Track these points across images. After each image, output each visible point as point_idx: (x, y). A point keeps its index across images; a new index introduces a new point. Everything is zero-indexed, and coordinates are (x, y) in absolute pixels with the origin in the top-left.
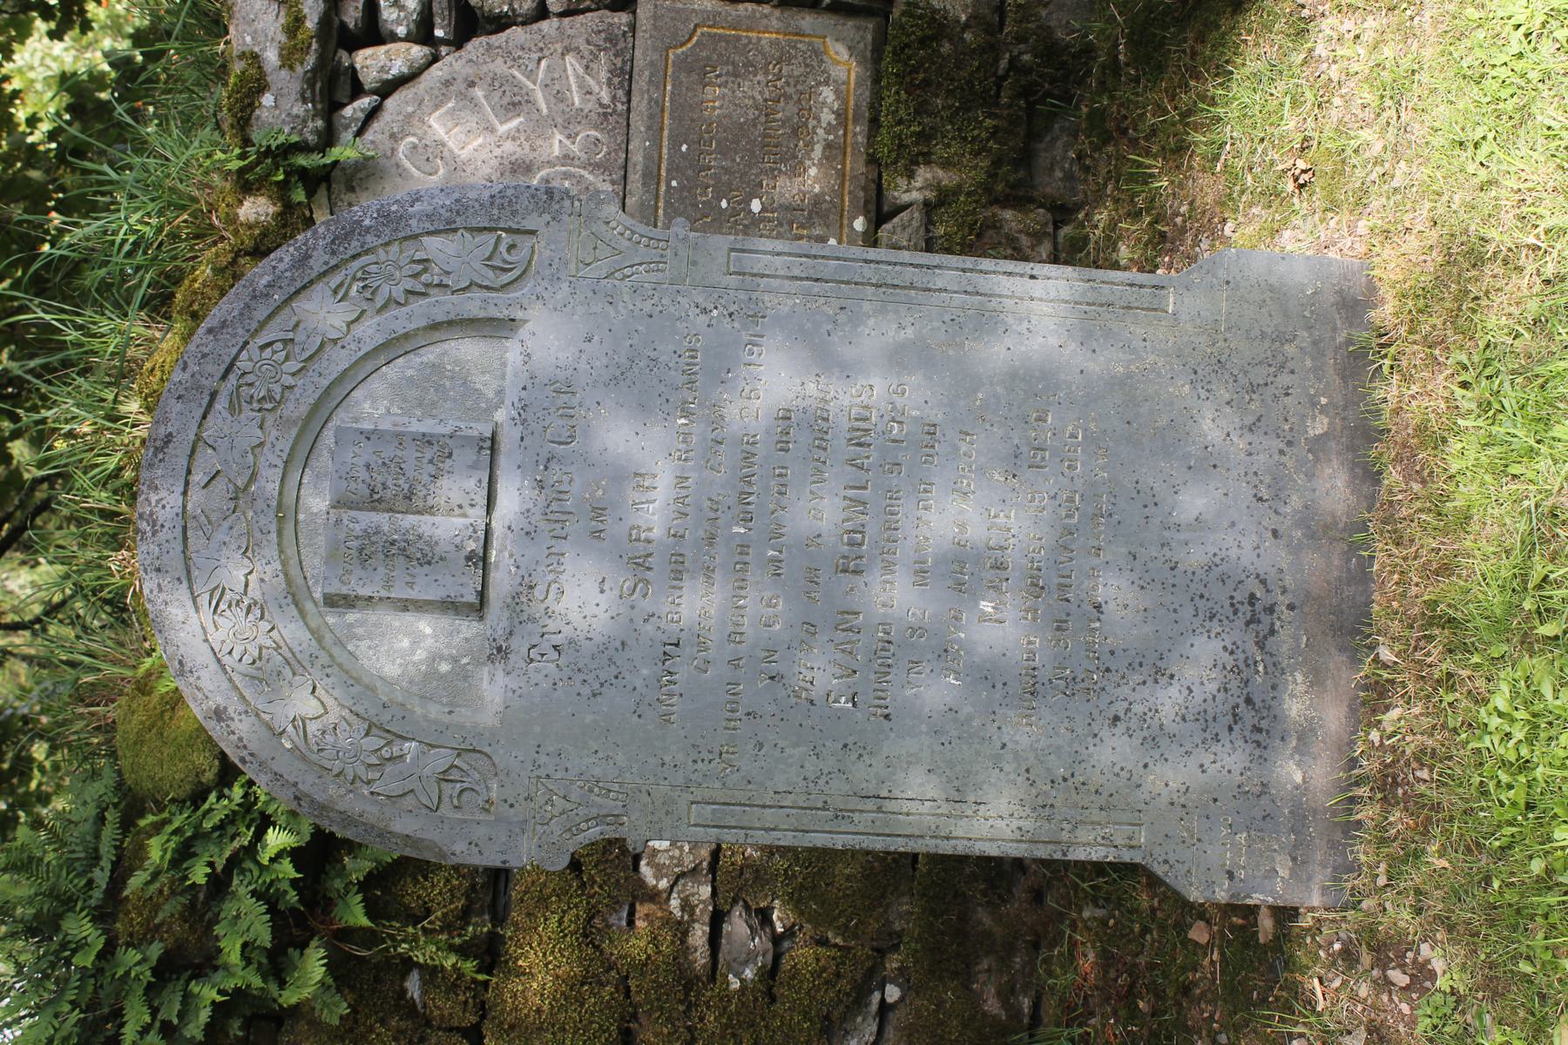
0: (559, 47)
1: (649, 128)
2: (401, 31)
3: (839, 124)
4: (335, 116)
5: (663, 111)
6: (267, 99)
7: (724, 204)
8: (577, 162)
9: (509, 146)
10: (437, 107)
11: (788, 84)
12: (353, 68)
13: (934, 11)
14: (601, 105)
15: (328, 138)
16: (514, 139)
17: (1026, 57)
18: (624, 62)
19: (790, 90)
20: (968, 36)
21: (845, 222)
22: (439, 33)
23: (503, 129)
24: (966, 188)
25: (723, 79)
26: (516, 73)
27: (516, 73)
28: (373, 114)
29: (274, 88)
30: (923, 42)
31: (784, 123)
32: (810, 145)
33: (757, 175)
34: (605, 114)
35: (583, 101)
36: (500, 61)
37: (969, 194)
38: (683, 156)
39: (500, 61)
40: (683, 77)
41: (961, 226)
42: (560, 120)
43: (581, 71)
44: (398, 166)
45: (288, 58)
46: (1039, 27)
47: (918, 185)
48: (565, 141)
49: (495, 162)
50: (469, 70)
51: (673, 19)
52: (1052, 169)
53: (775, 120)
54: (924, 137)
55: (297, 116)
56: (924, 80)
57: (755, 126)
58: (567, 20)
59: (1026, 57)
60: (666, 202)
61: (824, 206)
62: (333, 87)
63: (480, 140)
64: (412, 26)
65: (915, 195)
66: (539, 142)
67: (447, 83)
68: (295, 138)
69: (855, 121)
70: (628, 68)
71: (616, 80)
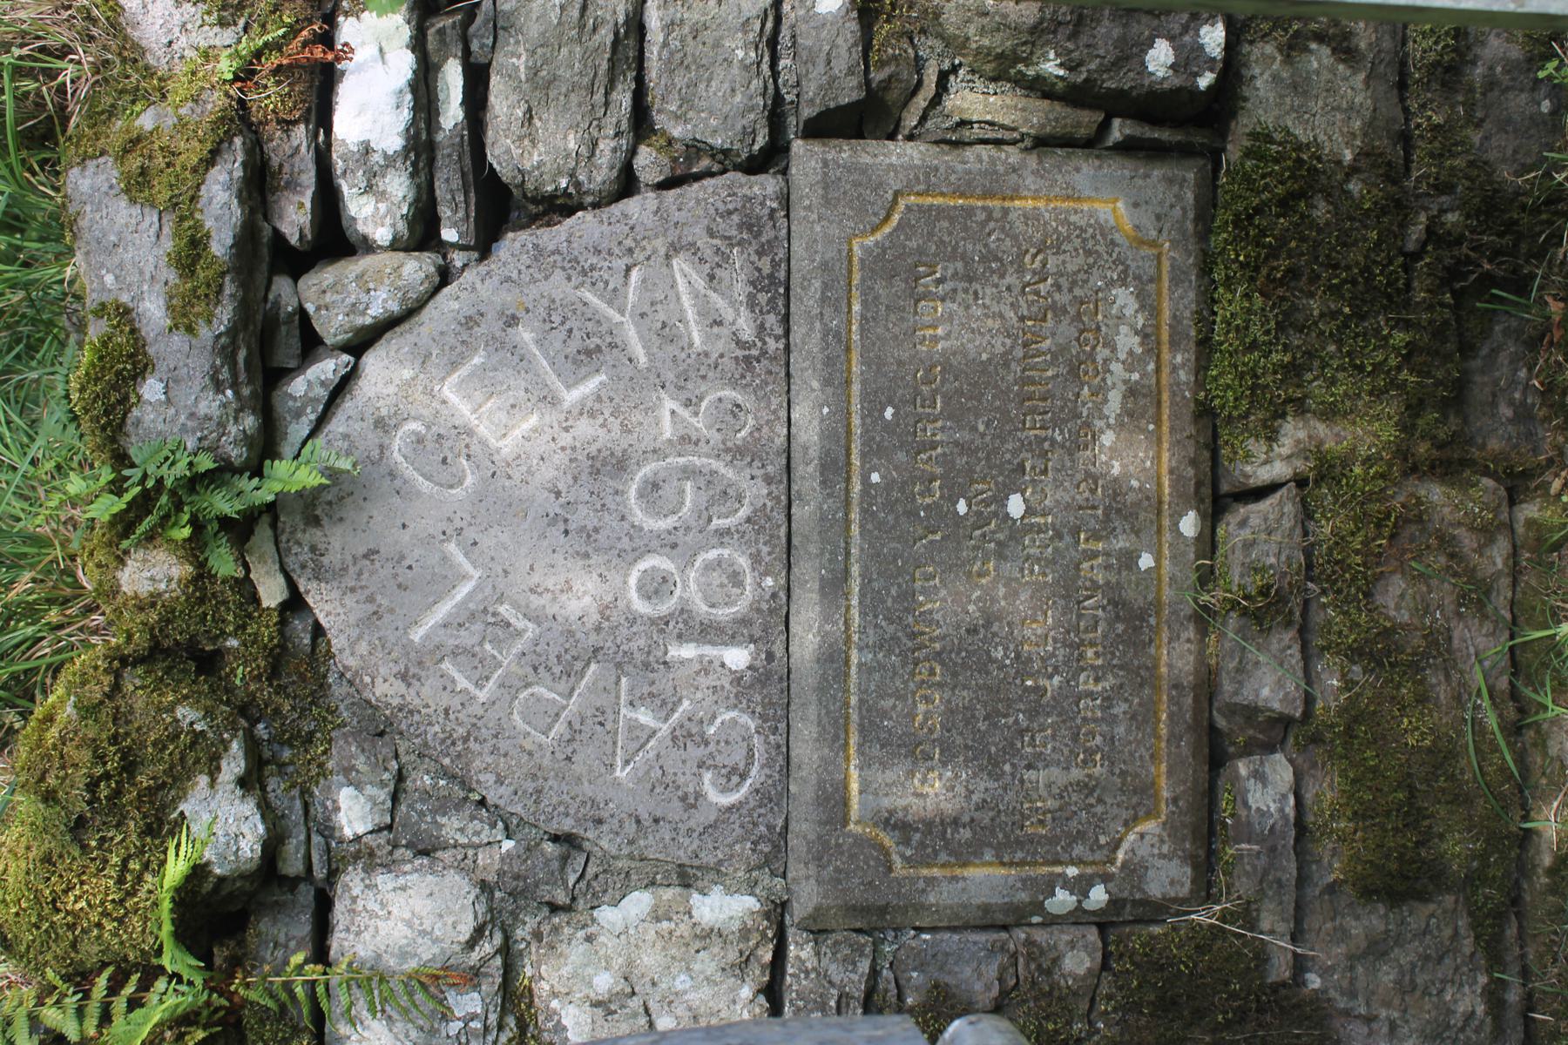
0: (660, 245)
1: (827, 382)
2: (382, 235)
3: (1148, 351)
4: (277, 397)
5: (848, 350)
6: (151, 389)
7: (962, 507)
9: (585, 428)
10: (454, 365)
11: (1058, 287)
12: (302, 312)
13: (1299, 147)
14: (740, 343)
15: (266, 446)
16: (592, 414)
17: (1452, 217)
18: (775, 265)
19: (1063, 298)
20: (1354, 187)
21: (1166, 522)
22: (449, 234)
23: (572, 397)
24: (1363, 451)
25: (949, 286)
26: (589, 296)
27: (589, 296)
28: (342, 387)
29: (162, 367)
30: (1285, 204)
31: (1055, 356)
32: (1100, 391)
33: (1015, 453)
34: (747, 359)
35: (707, 338)
36: (558, 276)
37: (1368, 461)
38: (887, 427)
39: (558, 276)
40: (880, 288)
41: (1361, 520)
42: (670, 376)
43: (700, 284)
44: (392, 475)
45: (183, 318)
46: (1471, 164)
47: (1285, 451)
48: (680, 410)
49: (560, 458)
50: (507, 297)
51: (856, 184)
52: (1494, 404)
53: (1039, 353)
54: (1293, 371)
55: (208, 418)
56: (1289, 271)
57: (1006, 365)
58: (671, 194)
59: (1452, 217)
60: (864, 511)
61: (1130, 498)
62: (266, 350)
63: (534, 420)
64: (402, 227)
65: (1279, 470)
66: (637, 417)
67: (470, 322)
68: (206, 463)
69: (1174, 345)
70: (782, 275)
71: (763, 298)
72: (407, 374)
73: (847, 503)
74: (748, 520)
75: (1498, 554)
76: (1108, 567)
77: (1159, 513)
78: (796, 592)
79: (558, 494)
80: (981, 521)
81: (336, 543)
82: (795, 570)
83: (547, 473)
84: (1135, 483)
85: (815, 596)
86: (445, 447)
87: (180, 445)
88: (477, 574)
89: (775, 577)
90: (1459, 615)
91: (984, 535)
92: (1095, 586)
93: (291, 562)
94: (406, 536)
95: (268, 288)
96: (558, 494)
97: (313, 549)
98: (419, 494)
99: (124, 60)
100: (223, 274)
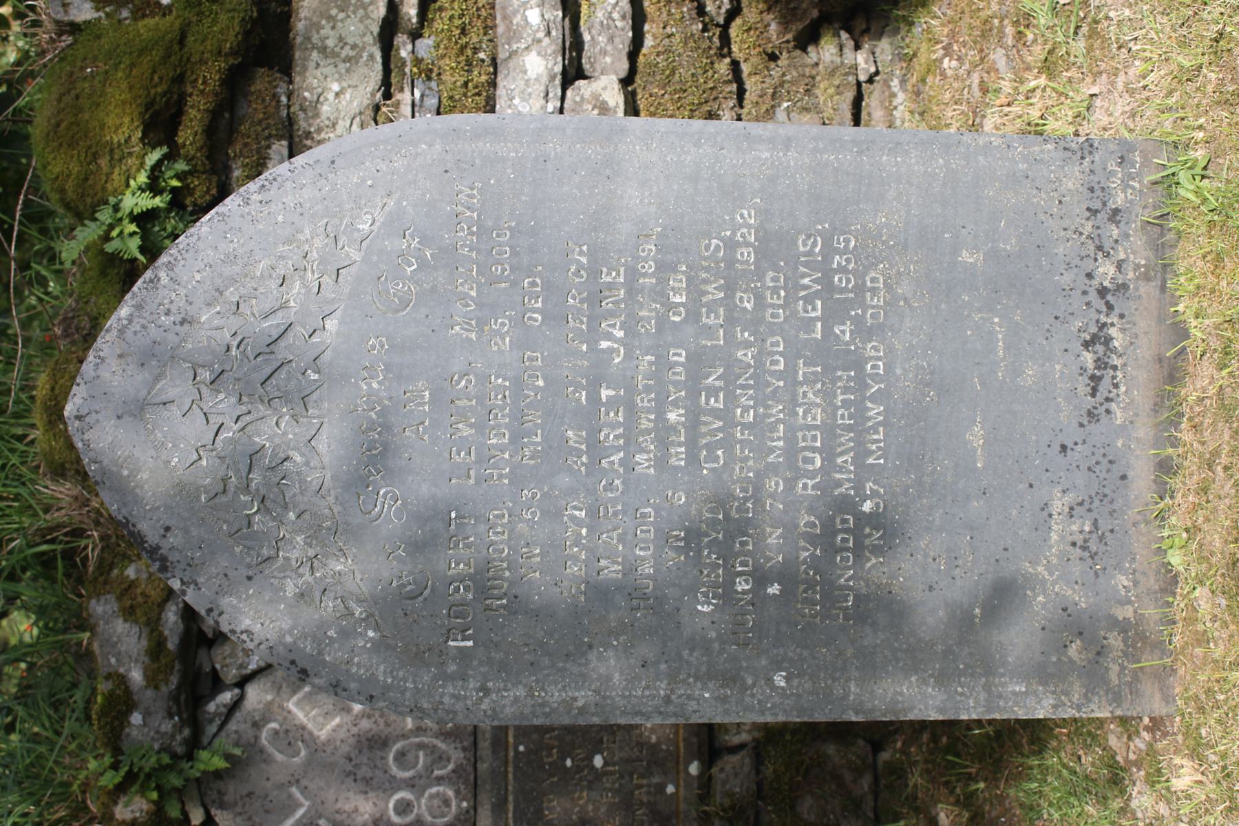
6: (136, 718)
7: (569, 763)
8: (429, 733)
10: (294, 692)
12: (214, 670)
15: (194, 744)
16: (369, 717)
21: (682, 767)
44: (262, 751)
45: (152, 680)
49: (352, 741)
55: (166, 733)
63: (337, 720)
72: (269, 697)
73: (506, 763)
74: (454, 771)
75: (866, 782)
76: (649, 793)
77: (678, 762)
78: (480, 810)
79: (351, 760)
80: (577, 769)
81: (231, 789)
82: (479, 798)
83: (345, 749)
84: (664, 747)
85: (489, 813)
86: (292, 736)
87: (152, 748)
88: (307, 803)
89: (468, 801)
90: (845, 817)
91: (580, 778)
92: (642, 804)
93: (207, 800)
94: (269, 784)
95: (195, 657)
96: (351, 760)
97: (219, 792)
98: (276, 762)
99: (117, 536)
100: (173, 661)
